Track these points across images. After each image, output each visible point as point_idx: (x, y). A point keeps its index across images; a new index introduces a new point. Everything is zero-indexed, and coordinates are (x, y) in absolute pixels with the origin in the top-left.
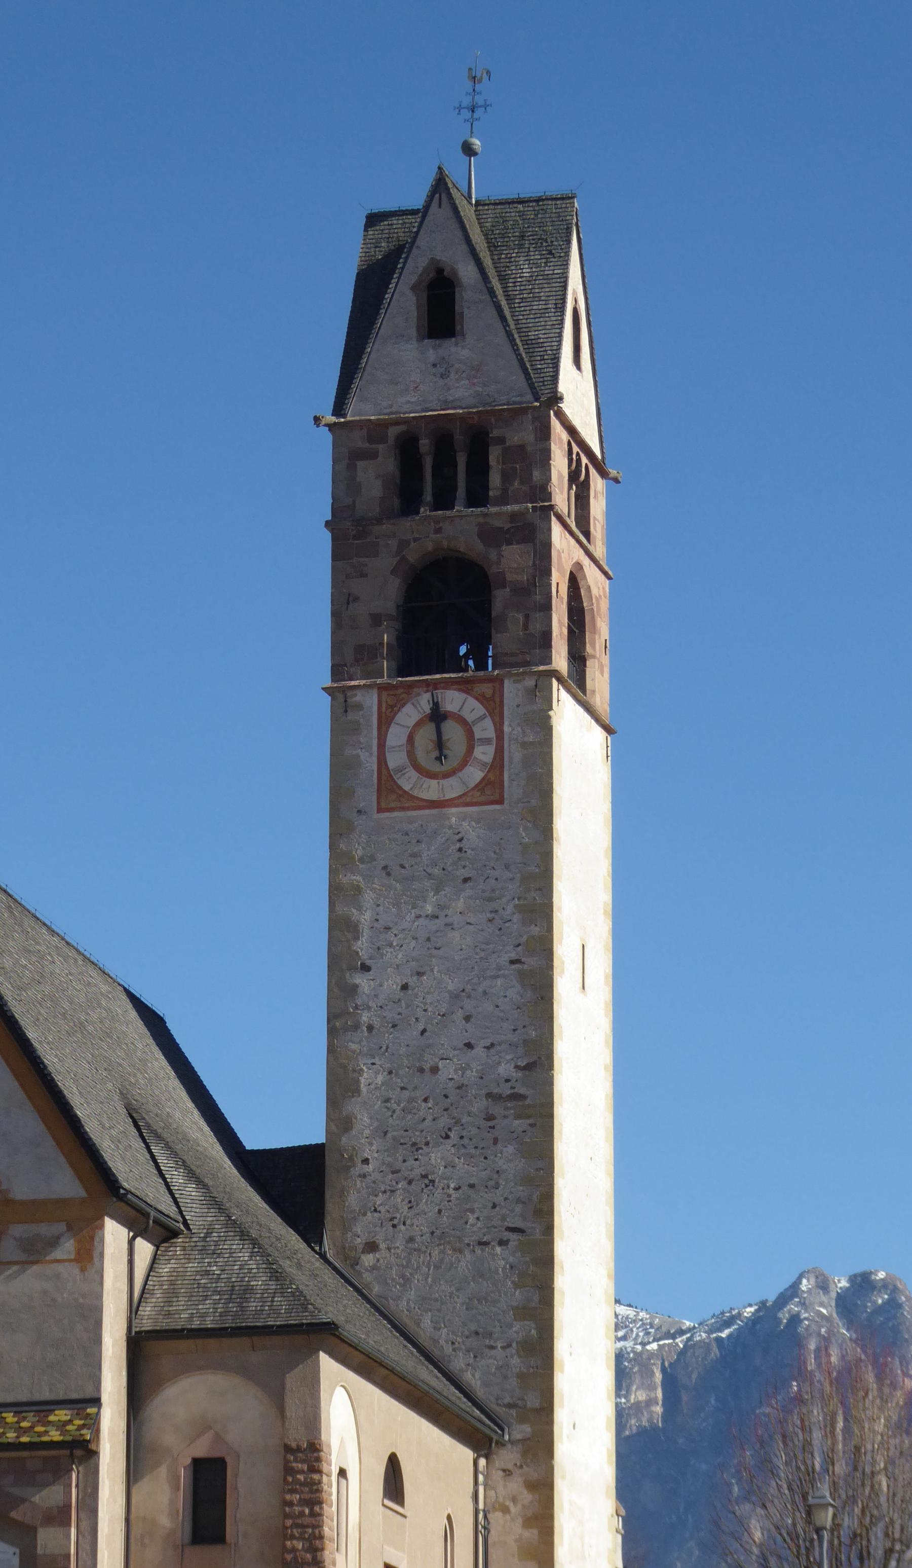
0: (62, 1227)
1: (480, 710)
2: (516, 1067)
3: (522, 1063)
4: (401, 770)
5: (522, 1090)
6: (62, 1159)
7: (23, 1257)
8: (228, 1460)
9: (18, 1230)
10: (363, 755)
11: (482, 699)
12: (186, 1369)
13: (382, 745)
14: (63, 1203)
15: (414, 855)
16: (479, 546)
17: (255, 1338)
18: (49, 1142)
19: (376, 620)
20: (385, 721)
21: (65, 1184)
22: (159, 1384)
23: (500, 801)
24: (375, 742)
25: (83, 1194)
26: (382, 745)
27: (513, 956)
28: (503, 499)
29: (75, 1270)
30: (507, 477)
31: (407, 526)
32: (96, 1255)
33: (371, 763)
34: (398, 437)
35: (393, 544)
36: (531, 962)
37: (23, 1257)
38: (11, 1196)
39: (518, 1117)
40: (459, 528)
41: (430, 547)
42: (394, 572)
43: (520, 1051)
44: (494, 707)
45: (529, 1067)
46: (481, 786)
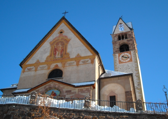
0: (89, 59)
1: (129, 54)
2: (137, 85)
3: (137, 84)
4: (121, 60)
5: (138, 87)
6: (89, 51)
7: (83, 63)
8: (116, 95)
9: (82, 60)
10: (117, 59)
11: (129, 53)
12: (108, 83)
13: (119, 58)
14: (89, 56)
15: (123, 67)
16: (127, 42)
17: (119, 77)
18: (87, 50)
19: (117, 48)
20: (119, 56)
21: (89, 53)
22: (104, 86)
23: (132, 61)
24: (118, 58)
25: (92, 55)
26: (119, 58)
27: (135, 75)
28: (129, 38)
29: (91, 64)
30: (129, 36)
31: (120, 41)
32: (94, 62)
33: (118, 60)
34: (118, 35)
35: (119, 43)
36: (137, 75)
37: (83, 63)
38: (81, 56)
39: (138, 90)
40: (125, 41)
41: (122, 42)
42: (119, 45)
43: (137, 83)
44: (130, 54)
45: (138, 85)
46: (130, 60)
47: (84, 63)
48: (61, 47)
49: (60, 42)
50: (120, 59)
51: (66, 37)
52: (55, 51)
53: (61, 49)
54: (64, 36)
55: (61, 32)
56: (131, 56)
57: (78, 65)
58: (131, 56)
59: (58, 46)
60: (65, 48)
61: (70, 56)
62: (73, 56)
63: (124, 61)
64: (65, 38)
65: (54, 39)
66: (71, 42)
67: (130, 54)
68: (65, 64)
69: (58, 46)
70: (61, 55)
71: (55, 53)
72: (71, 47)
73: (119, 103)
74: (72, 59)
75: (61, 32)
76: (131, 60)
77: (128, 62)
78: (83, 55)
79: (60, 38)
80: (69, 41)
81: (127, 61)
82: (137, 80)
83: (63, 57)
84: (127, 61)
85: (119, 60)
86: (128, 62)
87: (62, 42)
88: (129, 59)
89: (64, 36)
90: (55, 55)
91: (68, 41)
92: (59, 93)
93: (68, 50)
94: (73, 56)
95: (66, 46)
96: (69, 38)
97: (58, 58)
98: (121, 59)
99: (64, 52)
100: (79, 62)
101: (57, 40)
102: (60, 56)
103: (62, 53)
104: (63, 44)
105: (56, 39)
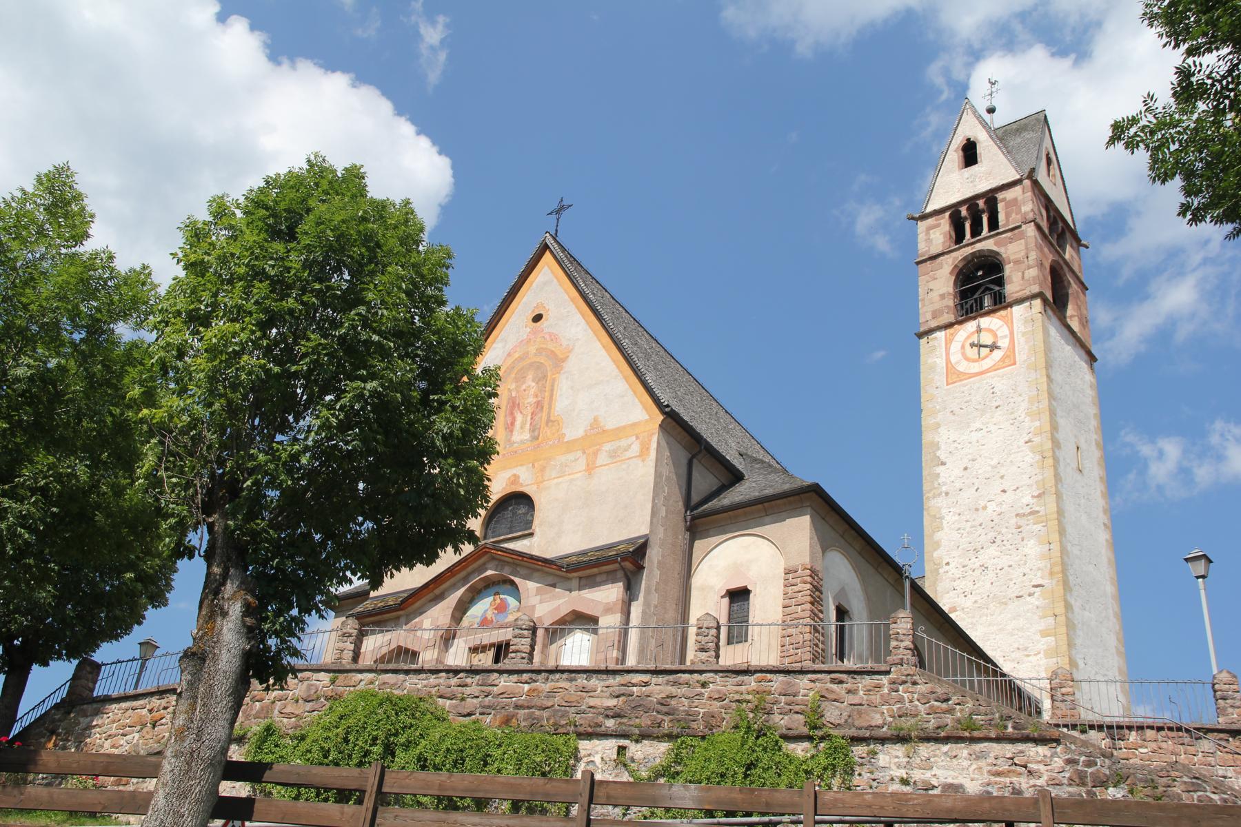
3: (1036, 494)
4: (958, 362)
10: (938, 360)
13: (948, 354)
14: (634, 425)
19: (942, 297)
23: (1014, 364)
26: (948, 354)
43: (1034, 487)
44: (1009, 323)
46: (1002, 359)
47: (614, 457)
48: (532, 391)
49: (531, 365)
50: (953, 359)
51: (554, 338)
52: (512, 414)
53: (532, 400)
54: (547, 337)
55: (537, 318)
56: (1012, 333)
57: (590, 469)
58: (1012, 333)
59: (524, 387)
60: (547, 394)
61: (564, 431)
62: (575, 431)
63: (975, 367)
64: (551, 346)
65: (509, 355)
66: (571, 365)
67: (1009, 323)
68: (543, 469)
69: (524, 387)
70: (532, 430)
71: (509, 420)
72: (572, 388)
73: (757, 629)
74: (570, 446)
75: (537, 318)
76: (1010, 359)
77: (994, 368)
78: (610, 424)
79: (532, 349)
80: (564, 360)
81: (987, 364)
82: (1037, 471)
83: (537, 438)
84: (987, 364)
85: (948, 361)
86: (994, 368)
87: (538, 366)
88: (997, 354)
89: (547, 337)
90: (512, 431)
91: (559, 361)
92: (328, 658)
93: (561, 405)
94: (575, 431)
95: (554, 380)
96: (565, 343)
97: (522, 442)
98: (999, 334)
99: (544, 415)
100: (596, 454)
101: (521, 359)
102: (526, 436)
103: (537, 418)
104: (542, 379)
105: (517, 355)
